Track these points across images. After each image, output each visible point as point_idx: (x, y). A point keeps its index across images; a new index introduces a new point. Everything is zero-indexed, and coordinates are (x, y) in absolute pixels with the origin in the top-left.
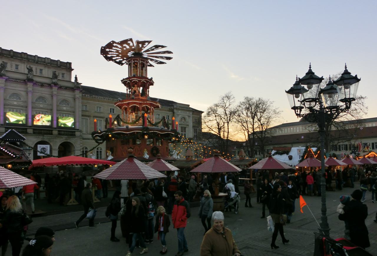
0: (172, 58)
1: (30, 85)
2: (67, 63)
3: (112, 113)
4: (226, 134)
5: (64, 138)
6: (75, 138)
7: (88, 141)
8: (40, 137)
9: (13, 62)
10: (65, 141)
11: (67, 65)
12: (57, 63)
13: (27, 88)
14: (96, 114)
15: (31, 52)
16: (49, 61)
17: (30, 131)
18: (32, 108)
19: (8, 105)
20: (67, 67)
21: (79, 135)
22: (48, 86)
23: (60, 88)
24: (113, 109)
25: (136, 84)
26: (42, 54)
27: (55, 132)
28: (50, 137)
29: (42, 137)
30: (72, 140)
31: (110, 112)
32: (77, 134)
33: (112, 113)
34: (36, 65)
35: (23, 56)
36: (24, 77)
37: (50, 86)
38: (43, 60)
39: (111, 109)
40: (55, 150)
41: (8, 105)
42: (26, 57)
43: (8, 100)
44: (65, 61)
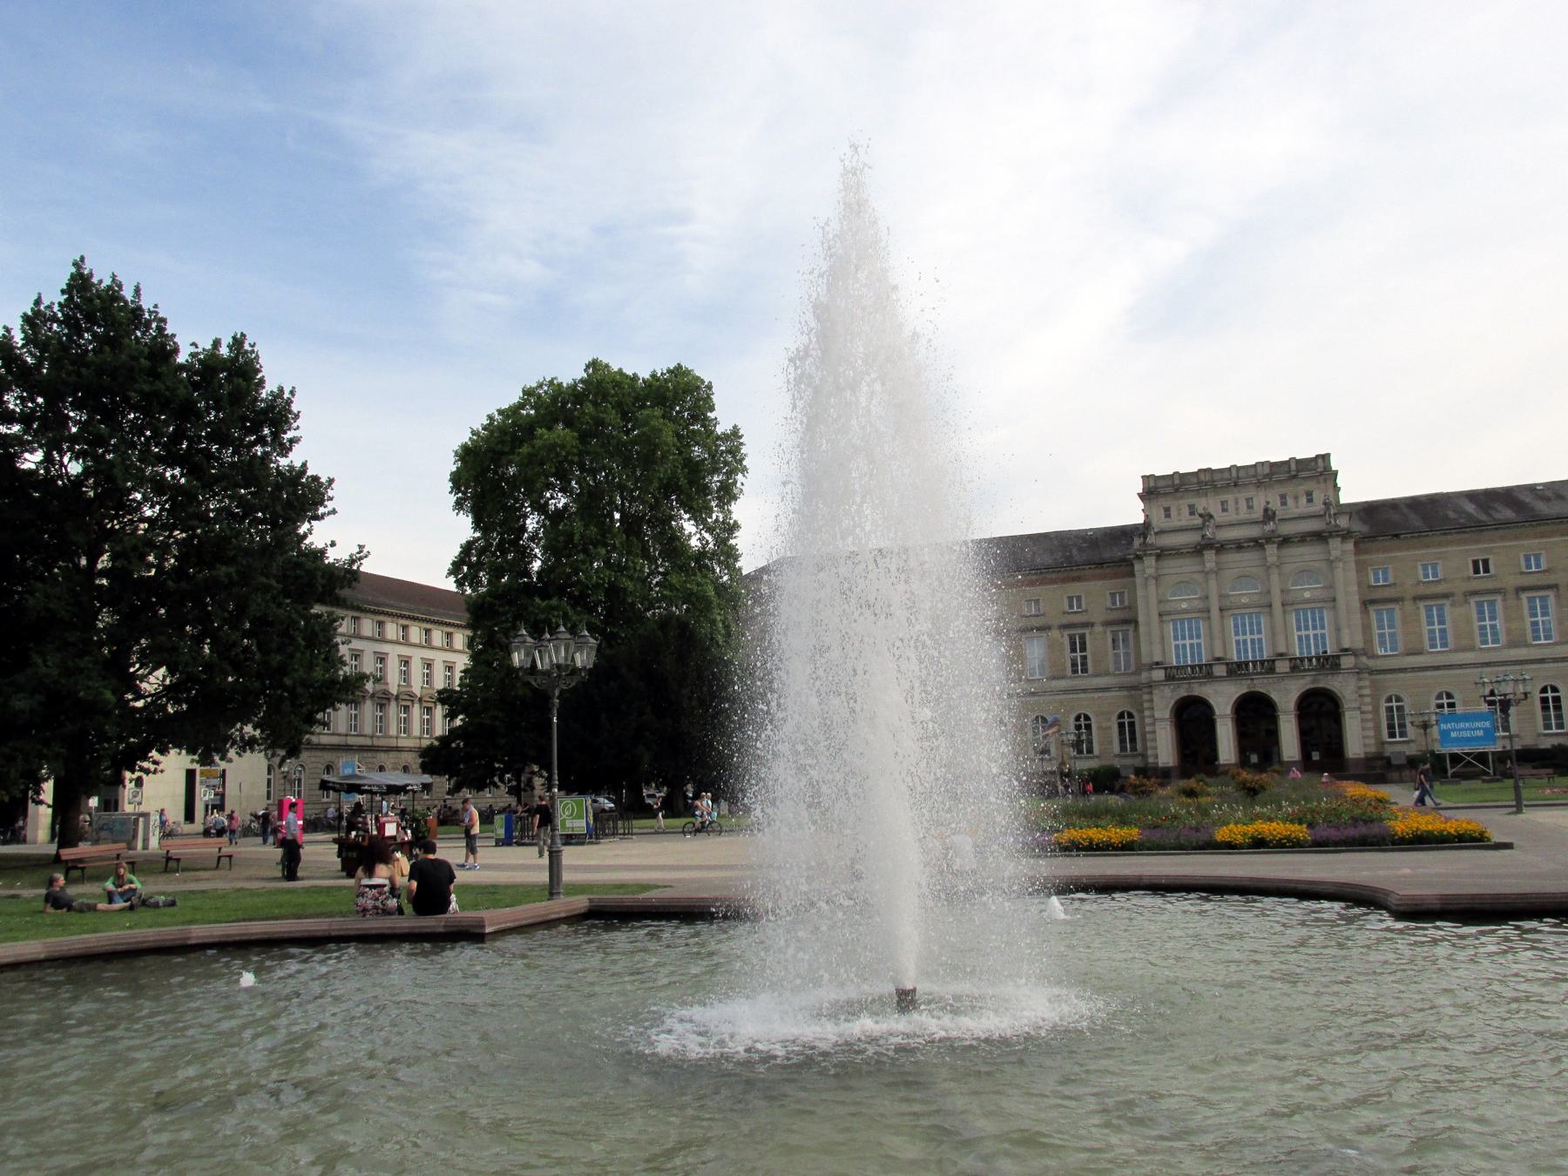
0: (40, 294)
1: (1210, 555)
2: (1317, 456)
3: (1482, 574)
4: (318, 730)
5: (1308, 678)
6: (1341, 676)
7: (1401, 675)
8: (1243, 682)
9: (1181, 502)
10: (1312, 686)
11: (1317, 463)
12: (1290, 468)
13: (1329, 552)
14: (1422, 590)
15: (1219, 461)
16: (1267, 471)
17: (1220, 670)
18: (1221, 610)
19: (1169, 613)
20: (1318, 470)
21: (1351, 666)
22: (1254, 546)
23: (1286, 541)
24: (1486, 562)
25: (538, 502)
26: (1246, 457)
27: (1282, 667)
28: (1265, 681)
29: (1249, 682)
30: (1335, 684)
31: (1471, 571)
32: (1347, 662)
33: (1482, 574)
34: (1235, 490)
35: (1202, 477)
36: (1192, 538)
37: (1257, 544)
38: (1252, 472)
39: (1475, 563)
40: (1285, 712)
41: (1169, 613)
42: (1208, 478)
43: (1168, 601)
44: (1310, 454)
